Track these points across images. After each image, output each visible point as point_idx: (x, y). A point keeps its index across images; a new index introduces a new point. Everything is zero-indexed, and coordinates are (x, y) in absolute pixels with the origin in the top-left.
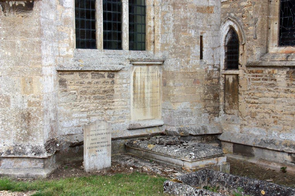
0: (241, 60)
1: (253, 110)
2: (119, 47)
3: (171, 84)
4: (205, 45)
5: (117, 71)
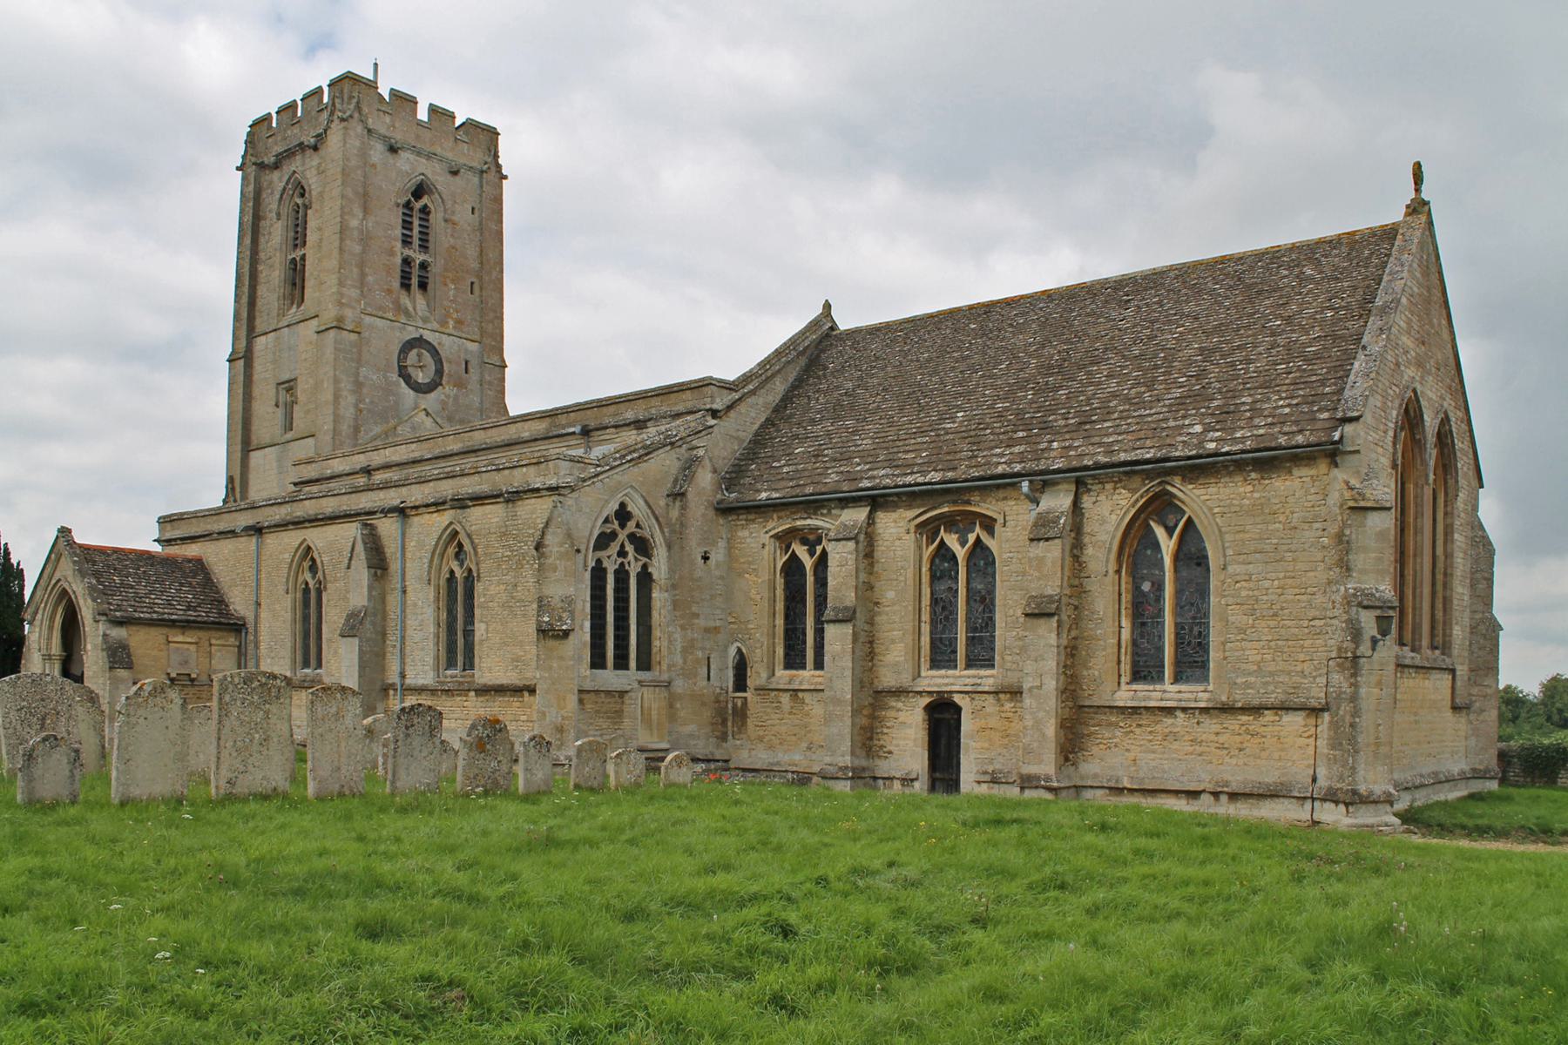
0: (749, 682)
1: (761, 733)
2: (626, 667)
3: (678, 706)
4: (712, 667)
5: (627, 692)
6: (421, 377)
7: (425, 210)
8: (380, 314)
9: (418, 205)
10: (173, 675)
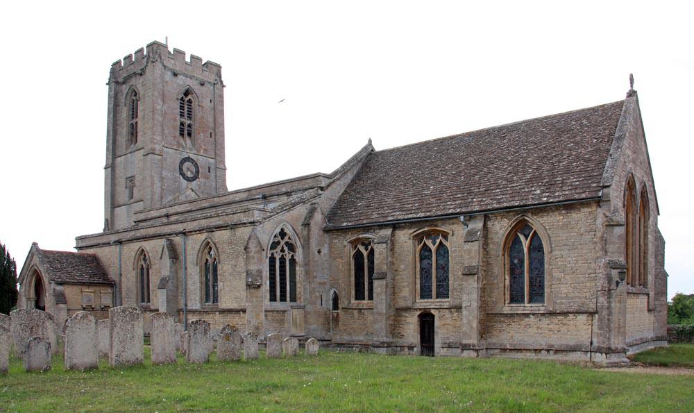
9: (186, 99)
10: (84, 306)
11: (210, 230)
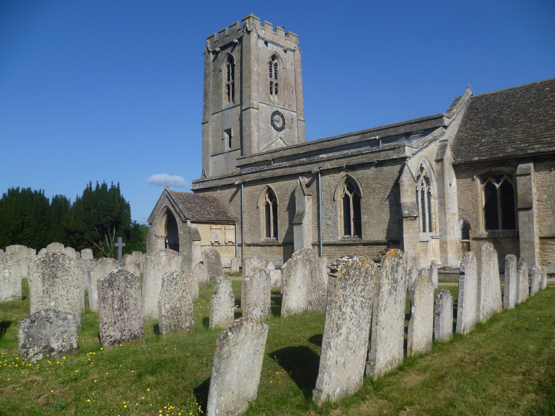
6: (279, 125)
7: (276, 65)
8: (264, 102)
9: (274, 62)
10: (213, 242)
11: (352, 168)
